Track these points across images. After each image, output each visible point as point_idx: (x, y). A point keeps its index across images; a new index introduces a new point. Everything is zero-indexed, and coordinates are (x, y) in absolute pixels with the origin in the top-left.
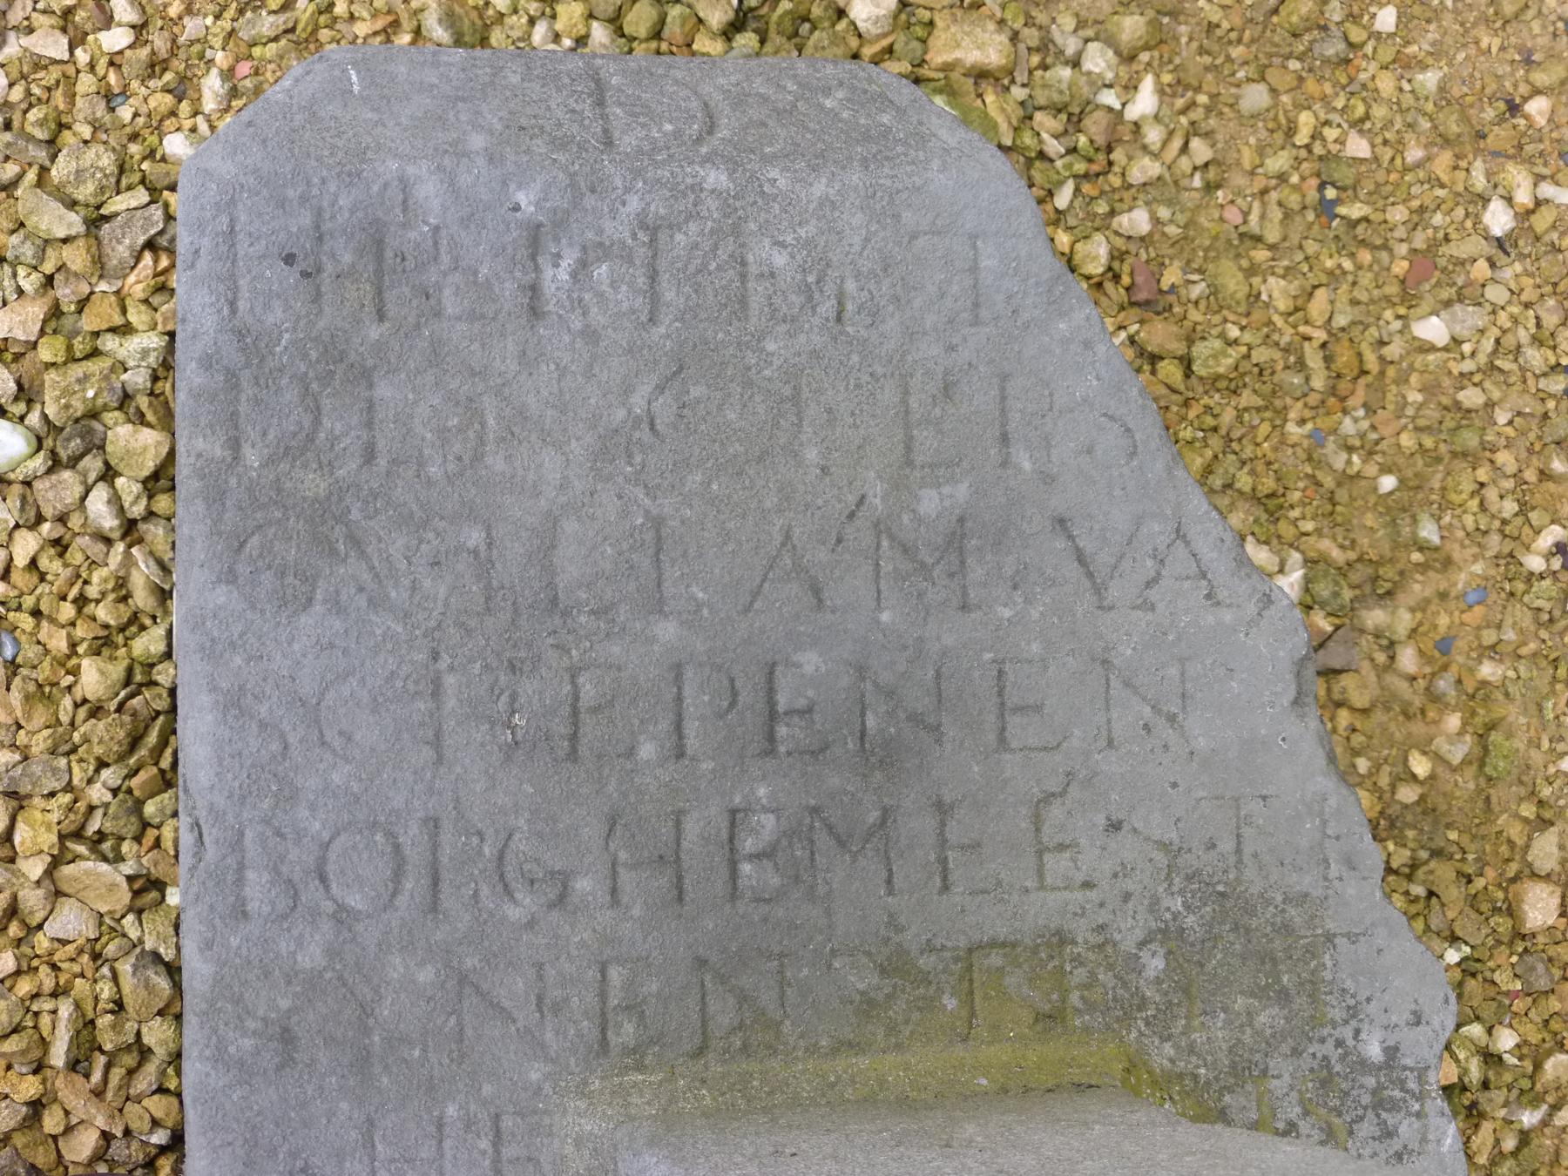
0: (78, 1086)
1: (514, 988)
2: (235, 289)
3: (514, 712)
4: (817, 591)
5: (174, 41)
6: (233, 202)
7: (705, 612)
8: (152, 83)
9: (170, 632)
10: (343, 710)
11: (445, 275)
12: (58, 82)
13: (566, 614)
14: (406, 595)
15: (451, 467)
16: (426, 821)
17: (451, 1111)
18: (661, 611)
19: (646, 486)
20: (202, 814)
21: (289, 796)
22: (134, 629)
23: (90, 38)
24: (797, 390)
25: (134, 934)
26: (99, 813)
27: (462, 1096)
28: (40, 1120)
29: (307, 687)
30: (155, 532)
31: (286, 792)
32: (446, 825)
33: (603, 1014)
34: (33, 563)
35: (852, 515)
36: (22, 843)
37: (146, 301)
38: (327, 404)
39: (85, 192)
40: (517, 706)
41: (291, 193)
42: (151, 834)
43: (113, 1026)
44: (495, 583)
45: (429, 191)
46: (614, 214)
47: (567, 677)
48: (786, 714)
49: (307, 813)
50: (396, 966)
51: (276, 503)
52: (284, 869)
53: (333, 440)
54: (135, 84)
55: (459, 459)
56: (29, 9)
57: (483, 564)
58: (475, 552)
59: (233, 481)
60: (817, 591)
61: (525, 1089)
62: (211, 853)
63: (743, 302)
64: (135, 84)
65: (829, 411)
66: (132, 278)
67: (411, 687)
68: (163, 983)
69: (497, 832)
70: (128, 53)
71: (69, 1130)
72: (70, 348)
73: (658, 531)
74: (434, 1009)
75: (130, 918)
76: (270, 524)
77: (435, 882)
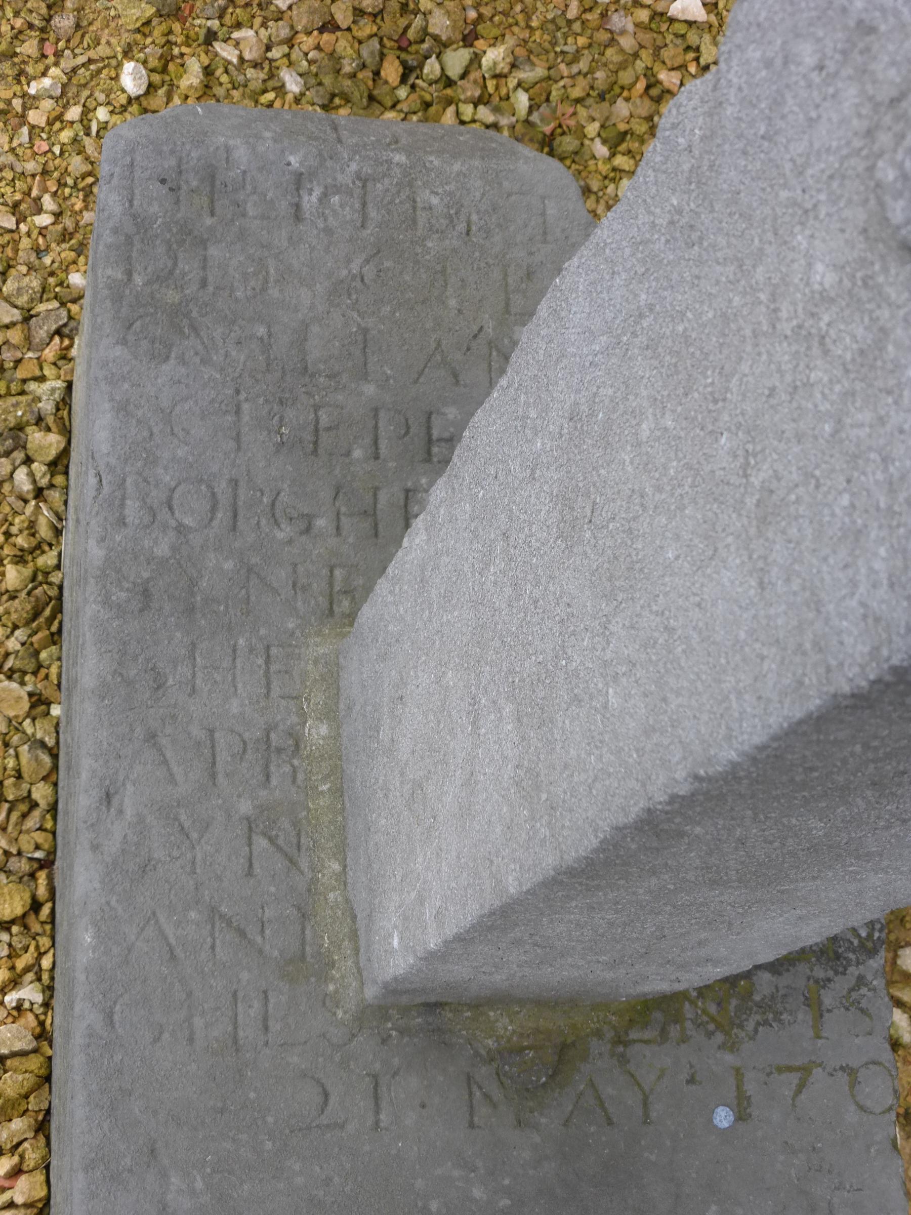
1: (280, 576)
2: (133, 194)
4: (455, 376)
5: (77, 224)
6: (133, 151)
7: (391, 381)
8: (64, 246)
9: (60, 554)
11: (248, 196)
13: (312, 376)
14: (222, 359)
15: (249, 293)
16: (231, 480)
17: (241, 642)
20: (102, 467)
22: (38, 552)
23: (29, 219)
24: (444, 269)
25: (30, 731)
26: (12, 657)
27: (247, 635)
30: (55, 496)
31: (151, 458)
32: (242, 484)
33: (331, 595)
35: (475, 336)
37: (55, 364)
38: (181, 255)
39: (22, 300)
41: (165, 148)
42: (43, 672)
43: (15, 785)
45: (241, 153)
46: (343, 171)
47: (312, 410)
48: (439, 440)
52: (148, 501)
53: (184, 274)
54: (53, 245)
55: (254, 289)
57: (266, 345)
58: (261, 339)
59: (127, 292)
60: (455, 376)
62: (106, 489)
63: (414, 221)
64: (53, 245)
65: (463, 281)
66: (47, 351)
67: (223, 407)
68: (46, 759)
69: (271, 490)
70: (50, 228)
72: (8, 388)
75: (28, 721)
77: (235, 516)
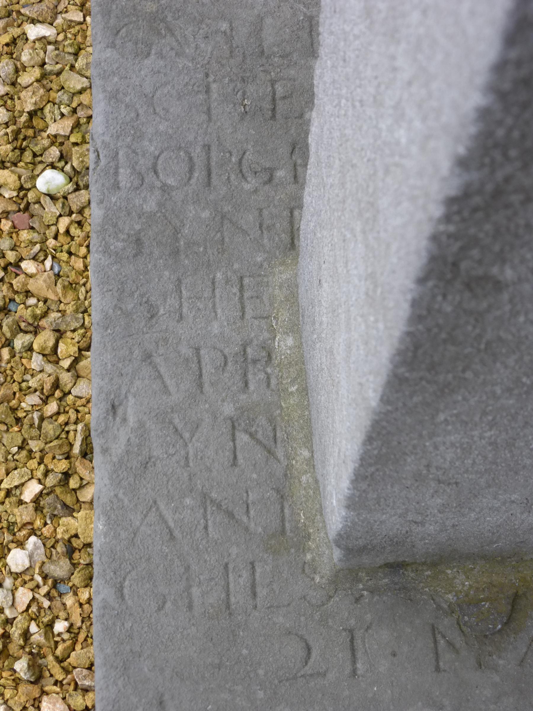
0: (87, 465)
3: (244, 100)
10: (165, 99)
12: (79, 31)
13: (268, 57)
14: (193, 51)
16: (204, 146)
17: (219, 275)
18: (313, 56)
19: (304, 4)
20: (99, 144)
21: (139, 136)
28: (68, 483)
29: (148, 89)
31: (138, 134)
32: (214, 148)
34: (67, 232)
36: (61, 352)
40: (246, 97)
44: (234, 45)
47: (269, 84)
49: (148, 143)
50: (191, 211)
51: (133, 14)
52: (137, 168)
56: (67, 3)
57: (229, 37)
58: (225, 33)
59: (114, 7)
61: (255, 265)
62: (103, 162)
67: (196, 88)
69: (238, 151)
71: (81, 487)
73: (311, 22)
74: (210, 229)
76: (131, 23)
77: (209, 174)
